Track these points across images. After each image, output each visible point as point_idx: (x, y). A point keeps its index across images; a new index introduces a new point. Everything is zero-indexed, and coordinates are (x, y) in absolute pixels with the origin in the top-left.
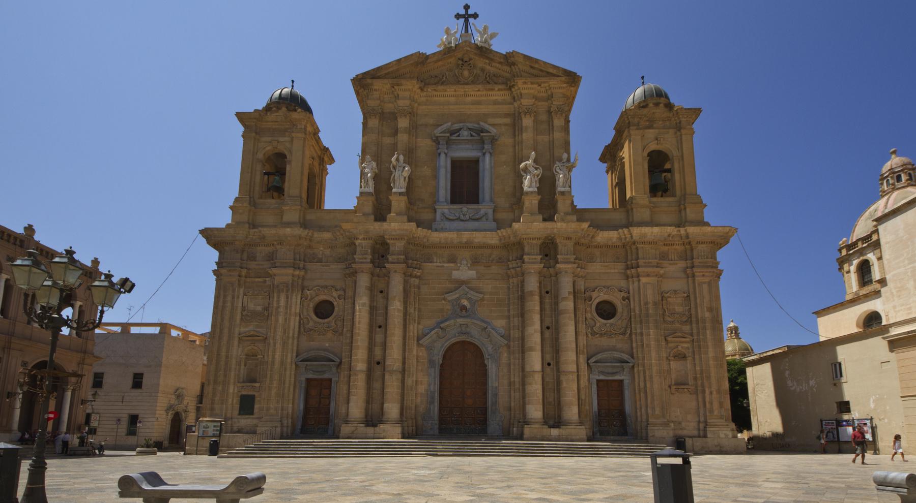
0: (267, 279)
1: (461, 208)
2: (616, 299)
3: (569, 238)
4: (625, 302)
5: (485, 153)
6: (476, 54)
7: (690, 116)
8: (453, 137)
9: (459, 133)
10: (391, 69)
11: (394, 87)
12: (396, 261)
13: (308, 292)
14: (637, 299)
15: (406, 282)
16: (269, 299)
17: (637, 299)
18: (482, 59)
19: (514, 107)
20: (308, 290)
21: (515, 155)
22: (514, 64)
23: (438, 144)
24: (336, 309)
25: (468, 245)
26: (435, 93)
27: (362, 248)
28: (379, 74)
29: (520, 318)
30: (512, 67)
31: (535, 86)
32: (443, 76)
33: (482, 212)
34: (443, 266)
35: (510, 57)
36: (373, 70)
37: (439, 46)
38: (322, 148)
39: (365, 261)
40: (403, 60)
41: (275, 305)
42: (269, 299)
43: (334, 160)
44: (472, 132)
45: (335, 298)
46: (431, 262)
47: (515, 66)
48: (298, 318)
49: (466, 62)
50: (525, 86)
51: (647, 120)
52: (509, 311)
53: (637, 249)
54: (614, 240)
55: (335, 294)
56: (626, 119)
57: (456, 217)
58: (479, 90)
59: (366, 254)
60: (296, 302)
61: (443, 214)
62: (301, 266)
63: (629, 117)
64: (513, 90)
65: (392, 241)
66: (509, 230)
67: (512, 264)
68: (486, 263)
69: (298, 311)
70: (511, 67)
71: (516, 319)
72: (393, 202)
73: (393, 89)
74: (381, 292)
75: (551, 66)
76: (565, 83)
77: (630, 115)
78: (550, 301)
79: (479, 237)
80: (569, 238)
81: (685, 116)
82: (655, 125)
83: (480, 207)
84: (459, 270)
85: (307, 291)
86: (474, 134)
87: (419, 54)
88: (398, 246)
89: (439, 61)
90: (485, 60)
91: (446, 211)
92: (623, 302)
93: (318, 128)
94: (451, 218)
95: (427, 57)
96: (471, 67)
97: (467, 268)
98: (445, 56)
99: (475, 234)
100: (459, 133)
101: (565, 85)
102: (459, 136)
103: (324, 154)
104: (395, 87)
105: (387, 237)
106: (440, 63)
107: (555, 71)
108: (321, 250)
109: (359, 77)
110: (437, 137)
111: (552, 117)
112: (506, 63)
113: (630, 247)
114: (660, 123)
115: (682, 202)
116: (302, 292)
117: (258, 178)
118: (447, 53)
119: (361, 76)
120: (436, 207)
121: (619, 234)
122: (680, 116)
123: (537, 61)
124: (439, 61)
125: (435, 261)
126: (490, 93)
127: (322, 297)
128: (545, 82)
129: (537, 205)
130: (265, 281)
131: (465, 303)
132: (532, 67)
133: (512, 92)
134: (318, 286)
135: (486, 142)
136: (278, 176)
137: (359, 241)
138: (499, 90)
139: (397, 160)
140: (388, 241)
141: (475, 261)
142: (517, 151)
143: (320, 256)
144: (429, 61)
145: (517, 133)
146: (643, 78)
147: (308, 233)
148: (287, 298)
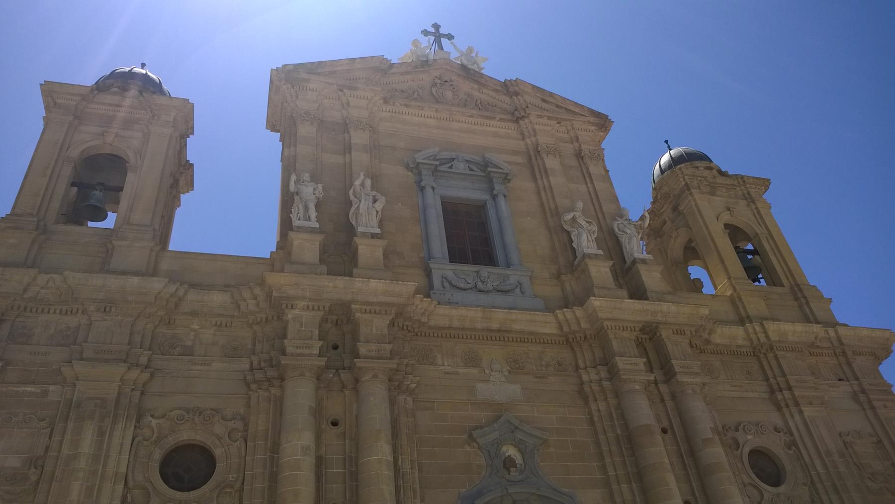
0: (52, 388)
1: (478, 272)
2: (775, 444)
3: (680, 332)
4: (792, 452)
5: (497, 195)
6: (459, 75)
7: (758, 187)
8: (443, 168)
9: (450, 164)
10: (340, 68)
11: (342, 91)
12: (373, 354)
13: (154, 422)
14: (809, 444)
15: (392, 402)
16: (50, 438)
17: (809, 444)
18: (467, 83)
19: (526, 144)
20: (152, 416)
21: (542, 204)
22: (517, 94)
23: (420, 174)
24: (220, 466)
25: (501, 335)
26: (404, 109)
27: (301, 325)
28: (319, 71)
29: (634, 484)
30: (515, 98)
31: (553, 122)
32: (414, 93)
33: (513, 280)
34: (457, 373)
35: (512, 85)
36: (312, 63)
37: (399, 59)
38: (183, 163)
39: (307, 351)
40: (357, 60)
41: (65, 451)
42: (50, 438)
43: (193, 186)
44: (471, 166)
45: (219, 438)
46: (432, 364)
47: (519, 97)
48: (120, 487)
49: (446, 81)
50: (540, 120)
51: (707, 185)
52: (603, 468)
53: (776, 357)
54: (740, 342)
55: (219, 428)
56: (682, 180)
57: (470, 286)
58: (472, 116)
59: (311, 338)
60: (122, 444)
61: (444, 278)
62: (144, 360)
63: (686, 177)
64: (521, 122)
65: (365, 316)
66: (579, 312)
67: (588, 373)
68: (537, 370)
69: (123, 469)
70: (511, 97)
71: (624, 487)
72: (360, 247)
73: (340, 93)
74: (335, 424)
75: (572, 103)
76: (593, 126)
77: (687, 175)
78: (622, 459)
79: (521, 321)
80: (680, 332)
81: (754, 186)
82: (717, 193)
83: (509, 272)
84: (488, 381)
85: (150, 419)
86: (475, 168)
87: (382, 59)
88: (377, 325)
89: (407, 73)
90: (471, 85)
91: (450, 274)
92: (789, 451)
93: (193, 128)
94: (462, 285)
95: (392, 66)
96: (454, 88)
97: (503, 379)
98: (417, 70)
99: (515, 315)
100: (450, 164)
101: (593, 128)
102: (451, 167)
103: (181, 173)
104: (345, 91)
105: (357, 307)
106: (408, 77)
107: (578, 109)
108: (195, 330)
109: (288, 68)
110: (419, 163)
111: (585, 164)
112: (505, 92)
113: (765, 354)
114: (724, 191)
115: (800, 295)
116: (138, 421)
117: (61, 187)
118: (419, 66)
119: (292, 68)
120: (432, 266)
121: (746, 331)
122: (748, 185)
123: (551, 95)
124: (407, 73)
125: (440, 361)
126: (488, 122)
127: (185, 435)
128: (566, 120)
129: (610, 275)
130: (45, 393)
131: (511, 451)
132: (544, 101)
133: (520, 126)
134: (180, 409)
135: (495, 181)
136: (101, 191)
137: (296, 312)
138: (501, 120)
139: (363, 185)
140: (358, 315)
141: (516, 368)
142: (544, 198)
143: (190, 343)
144: (394, 70)
145: (538, 176)
146: (666, 142)
147: (177, 290)
148: (101, 433)
